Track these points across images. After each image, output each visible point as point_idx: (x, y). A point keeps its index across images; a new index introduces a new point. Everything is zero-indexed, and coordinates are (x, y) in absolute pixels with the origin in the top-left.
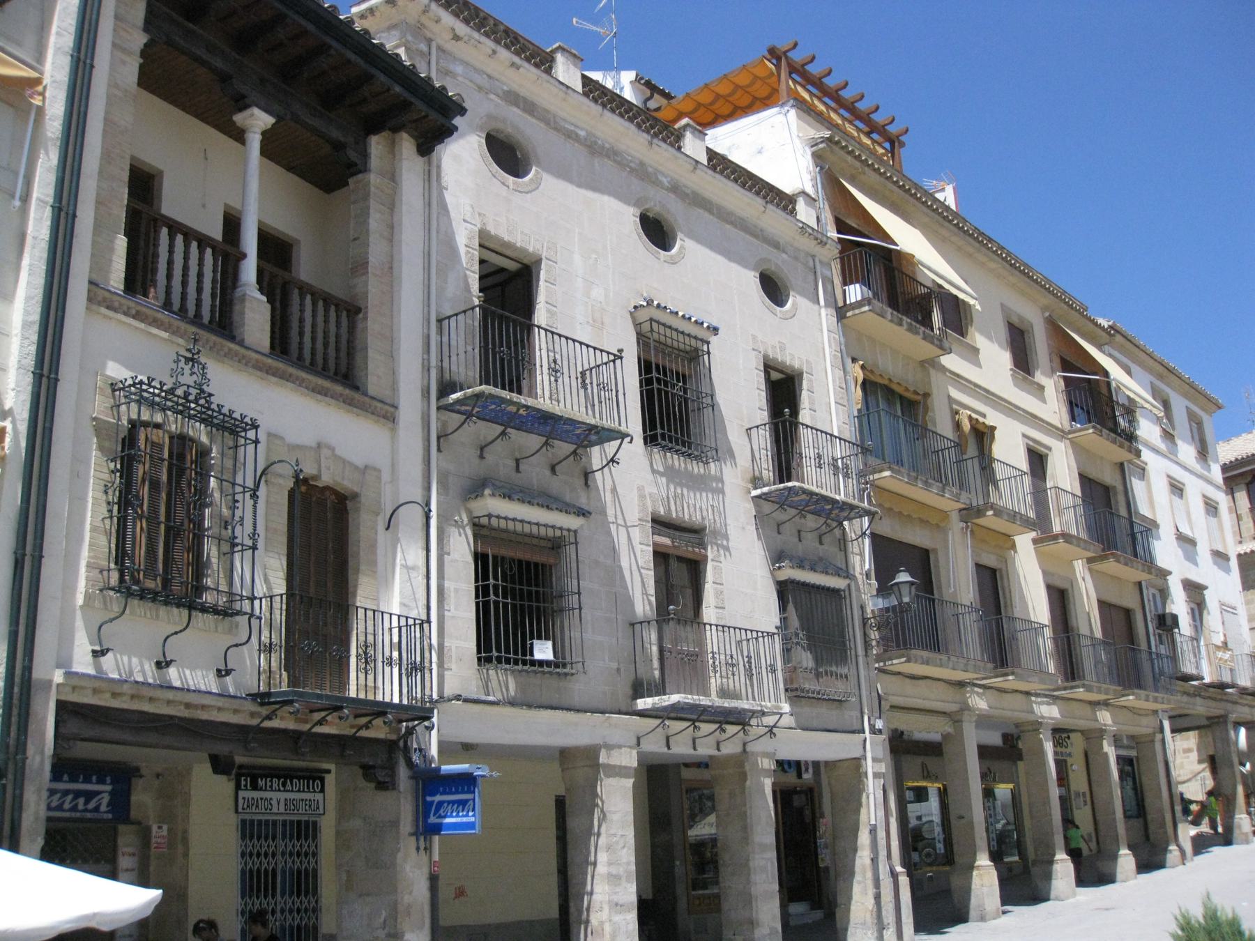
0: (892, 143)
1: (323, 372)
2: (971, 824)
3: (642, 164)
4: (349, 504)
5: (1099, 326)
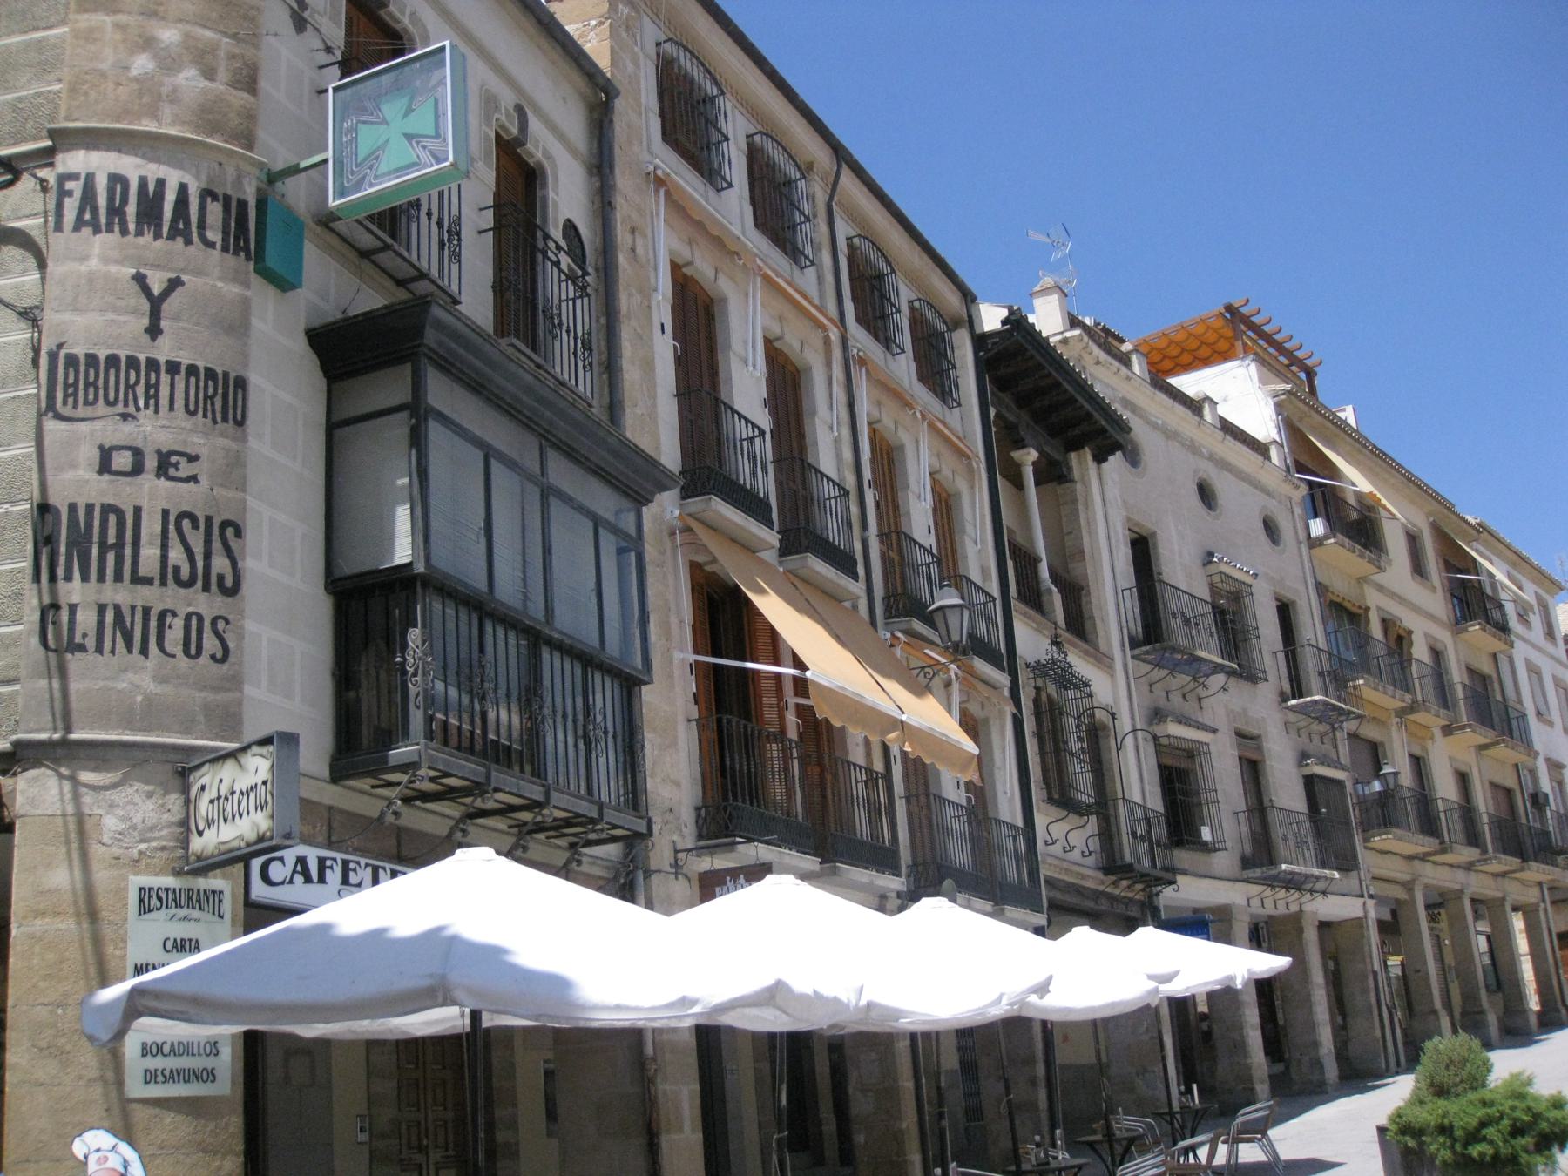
2: (1427, 978)
3: (1192, 440)
4: (1101, 733)
5: (1468, 523)
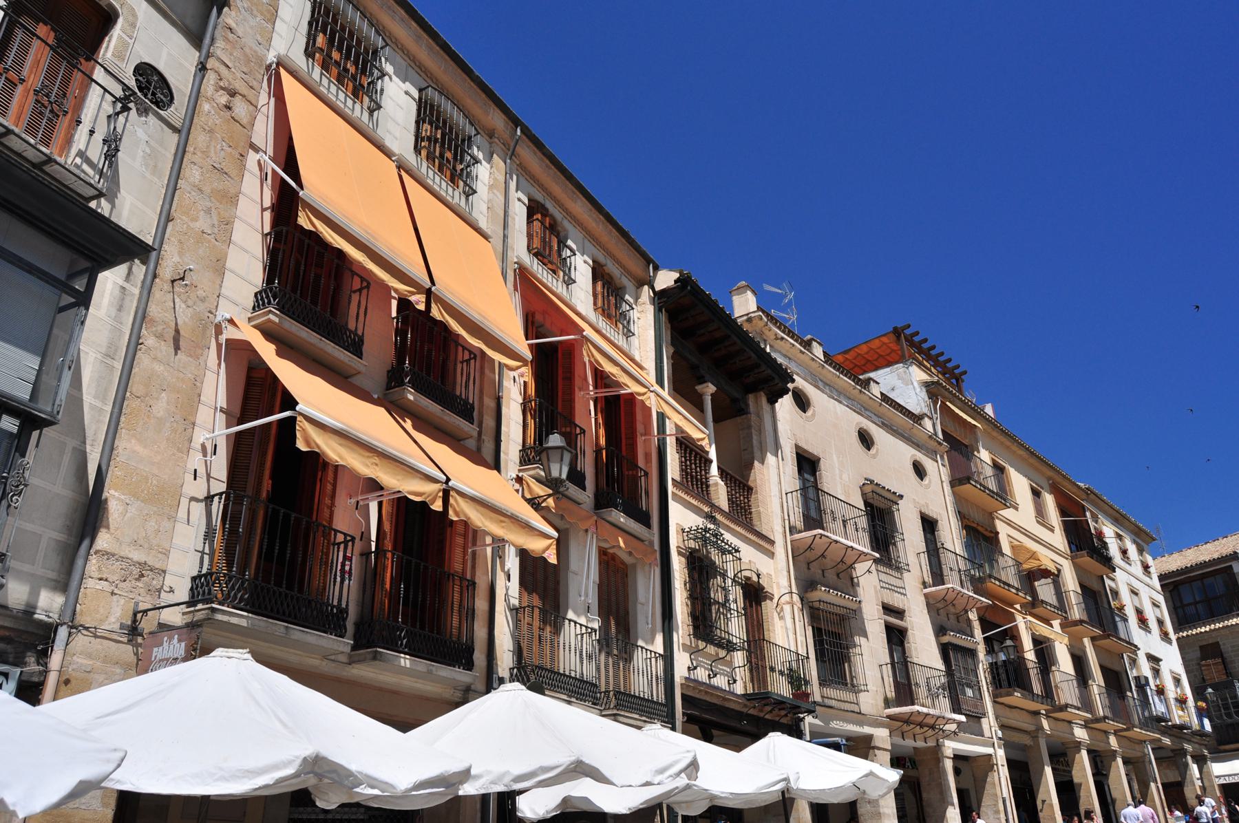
0: (957, 380)
1: (967, 500)
5: (1079, 487)
